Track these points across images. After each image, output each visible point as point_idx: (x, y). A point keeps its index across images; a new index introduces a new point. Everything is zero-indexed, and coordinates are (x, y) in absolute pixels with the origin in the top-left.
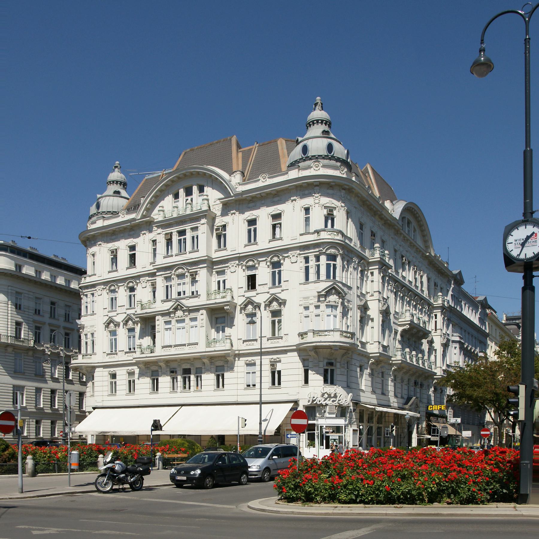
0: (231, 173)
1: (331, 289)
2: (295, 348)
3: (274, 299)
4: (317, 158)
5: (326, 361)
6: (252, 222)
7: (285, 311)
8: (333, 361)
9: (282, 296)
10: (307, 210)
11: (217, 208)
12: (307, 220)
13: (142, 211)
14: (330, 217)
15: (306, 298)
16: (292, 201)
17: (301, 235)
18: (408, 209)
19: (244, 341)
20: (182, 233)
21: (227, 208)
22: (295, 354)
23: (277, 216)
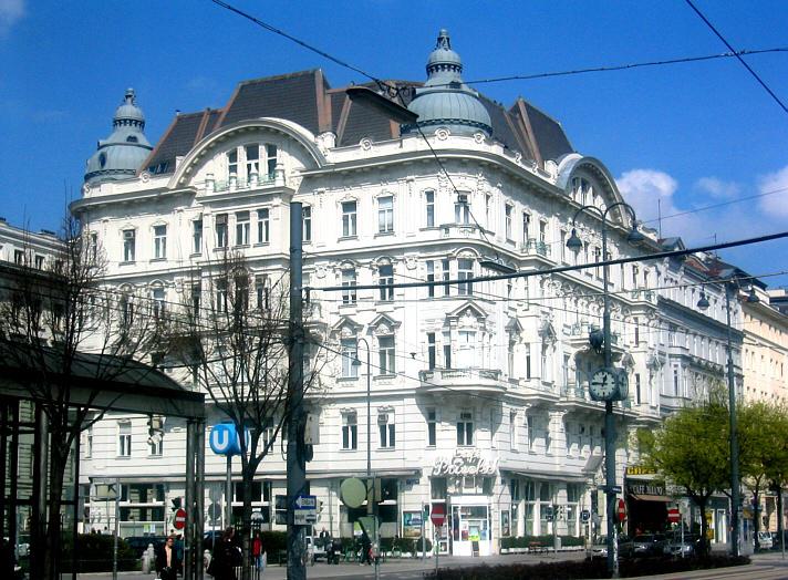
0: (317, 133)
1: (466, 309)
2: (414, 392)
3: (385, 319)
4: (442, 123)
5: (460, 411)
6: (350, 206)
7: (399, 335)
8: (470, 411)
9: (396, 316)
10: (430, 195)
11: (296, 182)
12: (431, 210)
13: (178, 177)
14: (463, 200)
15: (430, 321)
16: (408, 181)
17: (422, 230)
18: (585, 168)
19: (338, 380)
20: (243, 215)
21: (310, 182)
22: (413, 401)
23: (161, 230)
